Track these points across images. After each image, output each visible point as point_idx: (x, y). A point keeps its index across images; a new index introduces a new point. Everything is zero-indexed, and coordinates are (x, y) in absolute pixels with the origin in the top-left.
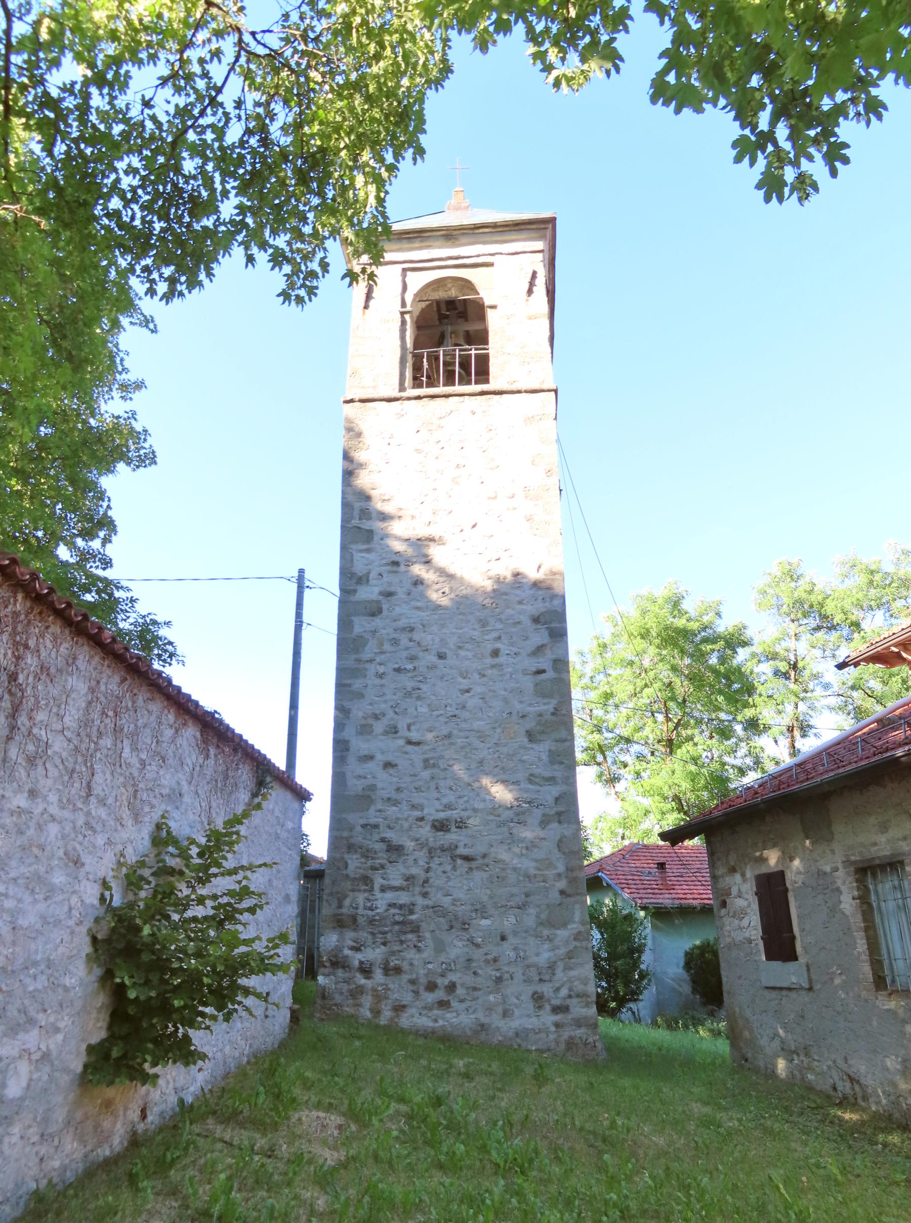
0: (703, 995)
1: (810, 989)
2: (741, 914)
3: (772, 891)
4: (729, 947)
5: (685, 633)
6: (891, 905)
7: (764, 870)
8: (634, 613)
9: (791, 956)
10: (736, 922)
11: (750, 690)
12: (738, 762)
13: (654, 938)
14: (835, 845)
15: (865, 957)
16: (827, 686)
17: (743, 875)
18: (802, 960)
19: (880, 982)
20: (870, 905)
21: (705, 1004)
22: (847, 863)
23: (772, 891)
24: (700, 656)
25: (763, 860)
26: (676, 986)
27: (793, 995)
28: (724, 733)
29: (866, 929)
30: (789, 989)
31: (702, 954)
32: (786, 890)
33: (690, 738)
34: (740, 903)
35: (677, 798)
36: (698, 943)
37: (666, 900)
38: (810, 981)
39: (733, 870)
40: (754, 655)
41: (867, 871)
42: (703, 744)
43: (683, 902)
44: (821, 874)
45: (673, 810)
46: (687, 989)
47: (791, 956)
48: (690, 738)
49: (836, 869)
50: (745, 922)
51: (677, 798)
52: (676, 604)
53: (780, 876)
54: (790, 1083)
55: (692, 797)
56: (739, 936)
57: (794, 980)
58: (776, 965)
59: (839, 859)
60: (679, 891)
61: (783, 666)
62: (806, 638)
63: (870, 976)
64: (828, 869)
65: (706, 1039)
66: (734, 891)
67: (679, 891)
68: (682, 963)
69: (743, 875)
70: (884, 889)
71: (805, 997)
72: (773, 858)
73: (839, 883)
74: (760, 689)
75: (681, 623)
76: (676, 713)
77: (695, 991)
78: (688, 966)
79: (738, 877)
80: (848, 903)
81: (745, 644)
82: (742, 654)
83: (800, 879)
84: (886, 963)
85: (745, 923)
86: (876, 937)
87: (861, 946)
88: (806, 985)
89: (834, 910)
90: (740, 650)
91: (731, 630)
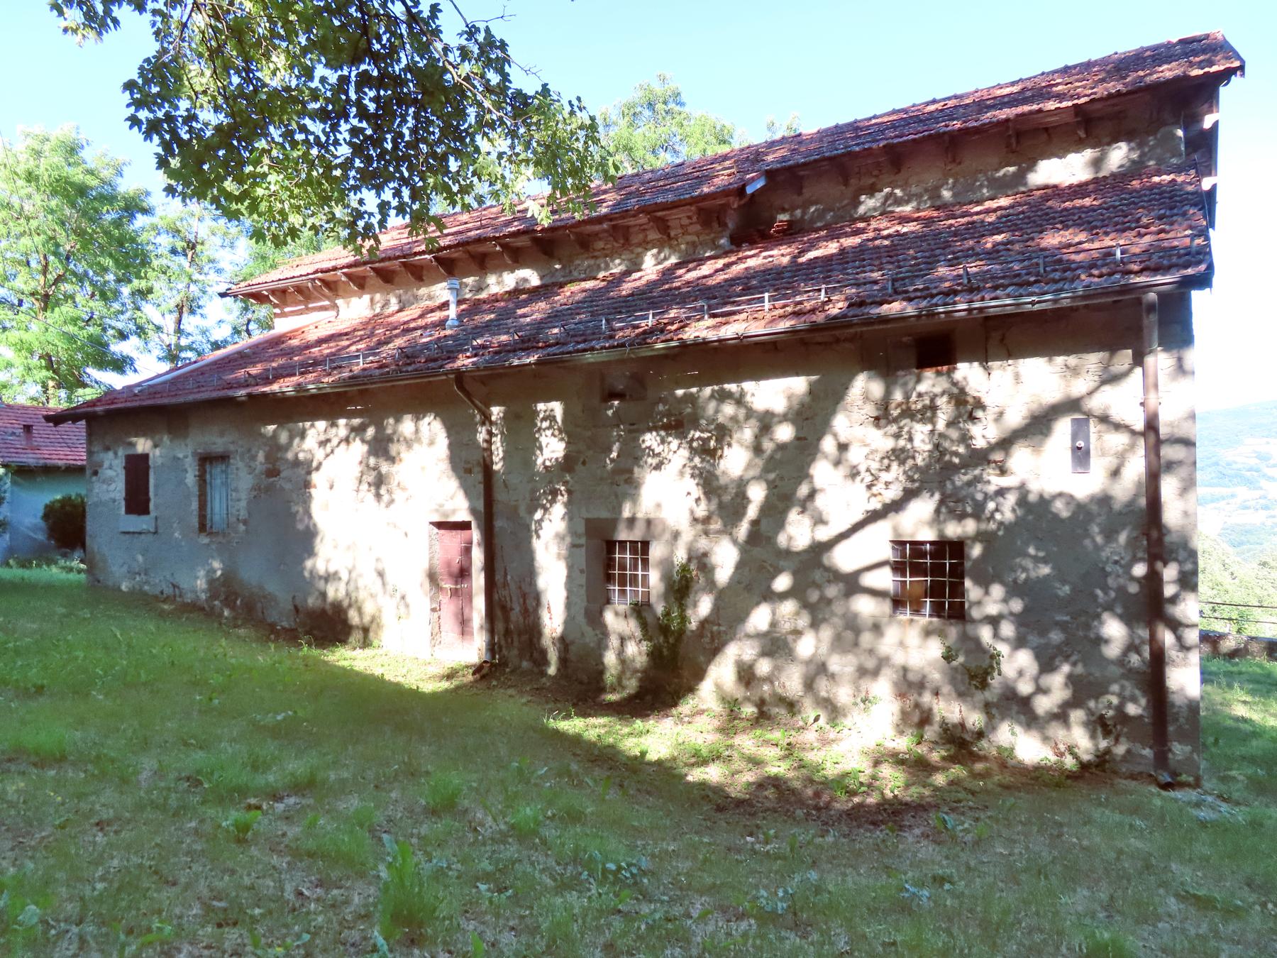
0: (57, 540)
1: (156, 533)
2: (109, 481)
3: (137, 469)
4: (96, 505)
5: (82, 190)
6: (218, 481)
7: (131, 452)
8: (21, 148)
9: (146, 511)
10: (105, 486)
11: (145, 262)
12: (120, 325)
13: (12, 493)
14: (189, 441)
15: (196, 513)
16: (219, 271)
17: (116, 454)
18: (153, 514)
19: (202, 528)
20: (205, 481)
21: (59, 547)
22: (194, 454)
23: (137, 469)
24: (94, 218)
25: (133, 445)
26: (32, 534)
27: (143, 536)
28: (105, 295)
29: (200, 496)
30: (140, 533)
31: (63, 507)
32: (148, 468)
33: (70, 297)
34: (110, 473)
35: (48, 357)
36: (58, 497)
37: (30, 459)
38: (156, 528)
39: (107, 449)
40: (154, 228)
41: (207, 460)
42: (85, 302)
43: (48, 461)
44: (176, 459)
45: (41, 367)
46: (41, 537)
47: (146, 511)
48: (70, 297)
49: (186, 457)
50: (112, 487)
51: (48, 357)
52: (72, 150)
53: (145, 457)
54: (132, 592)
55: (64, 356)
56: (105, 497)
57: (145, 527)
58: (133, 518)
59: (189, 451)
60: (45, 452)
61: (180, 245)
62: (208, 222)
63: (197, 525)
64: (181, 456)
65: (64, 571)
66: (106, 464)
67: (45, 452)
68: (41, 513)
69: (116, 454)
70: (216, 471)
71: (151, 537)
72: (142, 445)
73: (187, 466)
74: (155, 263)
75: (77, 175)
76: (56, 268)
77: (50, 537)
78: (46, 517)
79: (111, 454)
80: (191, 479)
81: (145, 211)
82: (141, 221)
83: (160, 461)
84: (209, 517)
85: (111, 486)
86: (205, 501)
87: (195, 505)
88: (152, 530)
89: (182, 482)
90: (139, 216)
91: (132, 194)
